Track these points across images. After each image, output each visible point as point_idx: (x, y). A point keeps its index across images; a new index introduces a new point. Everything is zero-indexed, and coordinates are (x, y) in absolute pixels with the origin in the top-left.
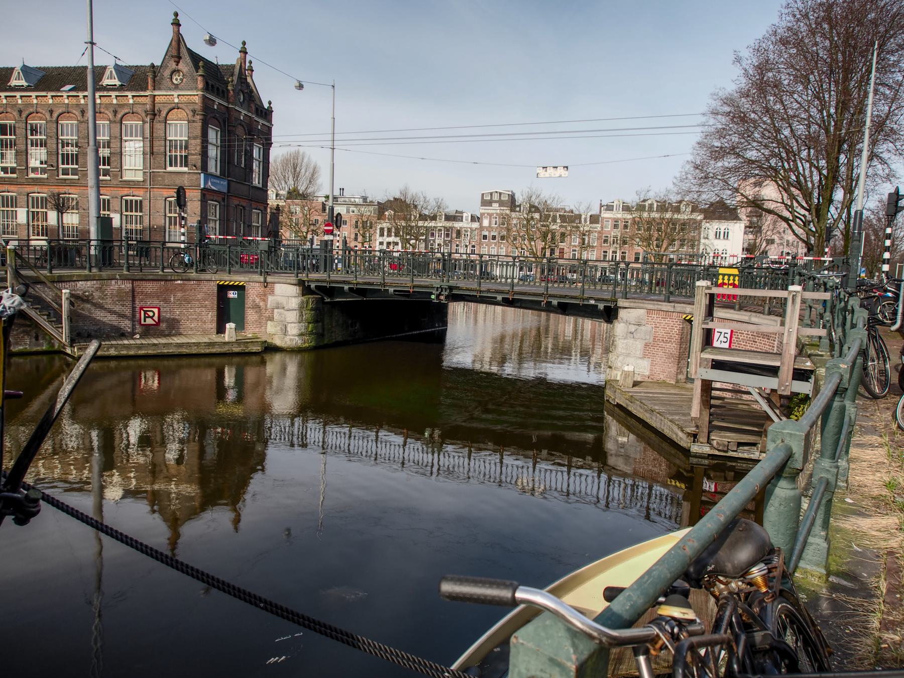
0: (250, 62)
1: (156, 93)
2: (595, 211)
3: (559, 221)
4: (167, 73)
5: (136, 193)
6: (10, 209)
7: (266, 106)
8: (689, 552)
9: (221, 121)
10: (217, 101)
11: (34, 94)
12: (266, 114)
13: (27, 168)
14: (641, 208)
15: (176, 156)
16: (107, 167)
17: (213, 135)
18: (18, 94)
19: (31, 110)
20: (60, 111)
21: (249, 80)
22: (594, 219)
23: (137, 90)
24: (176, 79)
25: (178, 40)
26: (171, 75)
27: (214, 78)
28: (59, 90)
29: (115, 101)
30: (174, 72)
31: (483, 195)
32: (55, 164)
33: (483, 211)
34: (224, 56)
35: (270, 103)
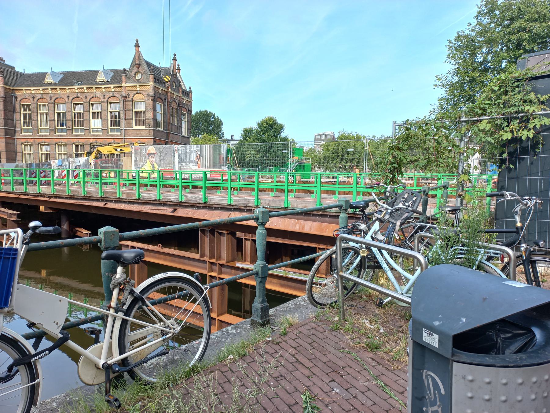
0: (179, 65)
5: (99, 141)
7: (188, 90)
9: (163, 99)
10: (161, 88)
11: (58, 88)
12: (187, 94)
15: (139, 120)
16: (118, 127)
17: (159, 106)
18: (49, 88)
19: (57, 96)
20: (73, 97)
21: (178, 76)
24: (138, 77)
25: (138, 55)
27: (156, 74)
28: (73, 85)
30: (137, 73)
31: (315, 136)
32: (71, 127)
33: (315, 146)
34: (162, 61)
35: (190, 88)
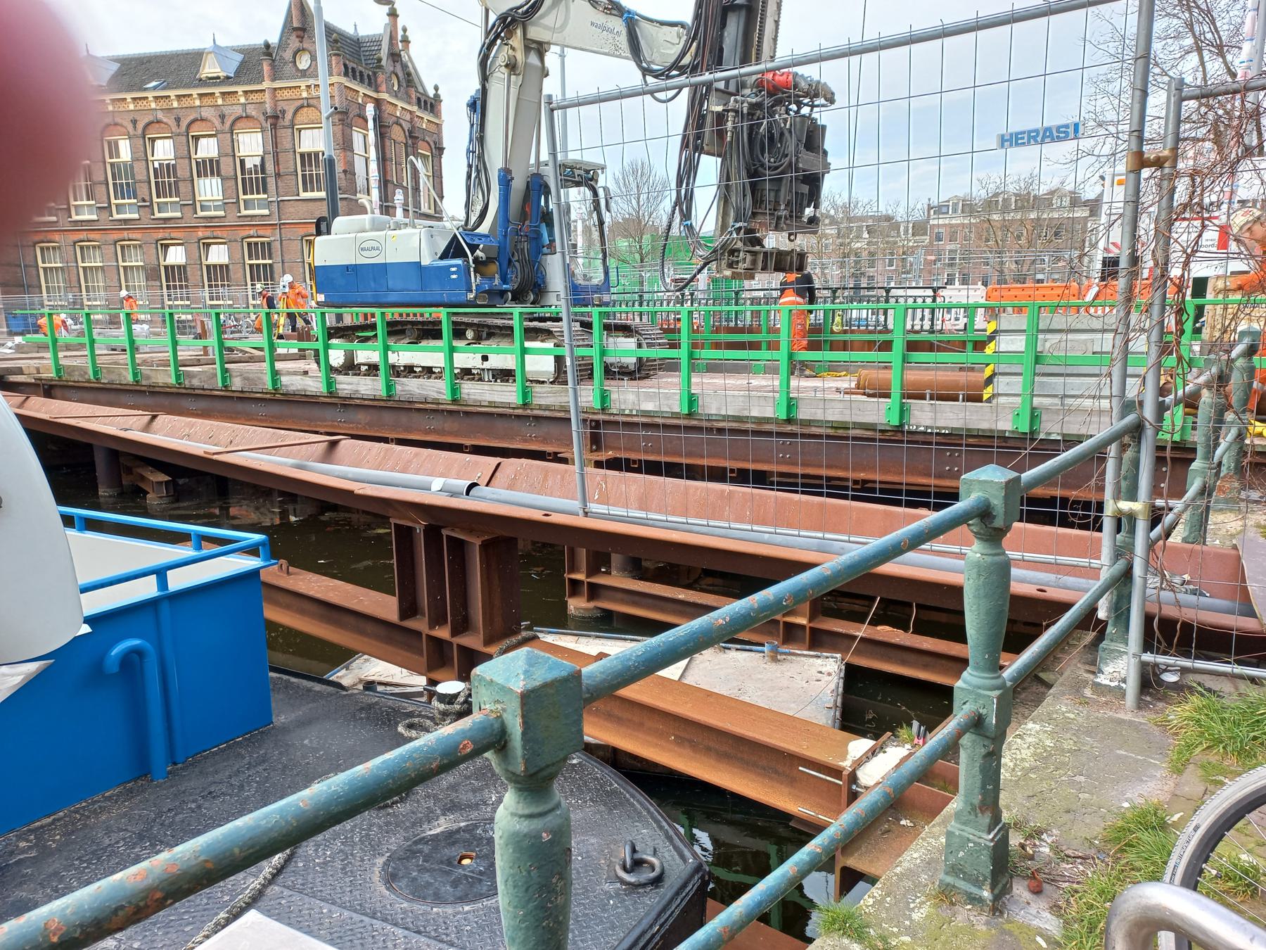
0: (405, 30)
1: (278, 84)
2: (918, 215)
3: (866, 235)
4: (288, 55)
6: (261, 261)
7: (431, 93)
8: (596, 720)
13: (194, 204)
14: (990, 204)
15: (311, 175)
20: (147, 121)
22: (919, 228)
23: (250, 82)
26: (294, 57)
27: (356, 58)
29: (175, 104)
32: (147, 198)
35: (436, 88)
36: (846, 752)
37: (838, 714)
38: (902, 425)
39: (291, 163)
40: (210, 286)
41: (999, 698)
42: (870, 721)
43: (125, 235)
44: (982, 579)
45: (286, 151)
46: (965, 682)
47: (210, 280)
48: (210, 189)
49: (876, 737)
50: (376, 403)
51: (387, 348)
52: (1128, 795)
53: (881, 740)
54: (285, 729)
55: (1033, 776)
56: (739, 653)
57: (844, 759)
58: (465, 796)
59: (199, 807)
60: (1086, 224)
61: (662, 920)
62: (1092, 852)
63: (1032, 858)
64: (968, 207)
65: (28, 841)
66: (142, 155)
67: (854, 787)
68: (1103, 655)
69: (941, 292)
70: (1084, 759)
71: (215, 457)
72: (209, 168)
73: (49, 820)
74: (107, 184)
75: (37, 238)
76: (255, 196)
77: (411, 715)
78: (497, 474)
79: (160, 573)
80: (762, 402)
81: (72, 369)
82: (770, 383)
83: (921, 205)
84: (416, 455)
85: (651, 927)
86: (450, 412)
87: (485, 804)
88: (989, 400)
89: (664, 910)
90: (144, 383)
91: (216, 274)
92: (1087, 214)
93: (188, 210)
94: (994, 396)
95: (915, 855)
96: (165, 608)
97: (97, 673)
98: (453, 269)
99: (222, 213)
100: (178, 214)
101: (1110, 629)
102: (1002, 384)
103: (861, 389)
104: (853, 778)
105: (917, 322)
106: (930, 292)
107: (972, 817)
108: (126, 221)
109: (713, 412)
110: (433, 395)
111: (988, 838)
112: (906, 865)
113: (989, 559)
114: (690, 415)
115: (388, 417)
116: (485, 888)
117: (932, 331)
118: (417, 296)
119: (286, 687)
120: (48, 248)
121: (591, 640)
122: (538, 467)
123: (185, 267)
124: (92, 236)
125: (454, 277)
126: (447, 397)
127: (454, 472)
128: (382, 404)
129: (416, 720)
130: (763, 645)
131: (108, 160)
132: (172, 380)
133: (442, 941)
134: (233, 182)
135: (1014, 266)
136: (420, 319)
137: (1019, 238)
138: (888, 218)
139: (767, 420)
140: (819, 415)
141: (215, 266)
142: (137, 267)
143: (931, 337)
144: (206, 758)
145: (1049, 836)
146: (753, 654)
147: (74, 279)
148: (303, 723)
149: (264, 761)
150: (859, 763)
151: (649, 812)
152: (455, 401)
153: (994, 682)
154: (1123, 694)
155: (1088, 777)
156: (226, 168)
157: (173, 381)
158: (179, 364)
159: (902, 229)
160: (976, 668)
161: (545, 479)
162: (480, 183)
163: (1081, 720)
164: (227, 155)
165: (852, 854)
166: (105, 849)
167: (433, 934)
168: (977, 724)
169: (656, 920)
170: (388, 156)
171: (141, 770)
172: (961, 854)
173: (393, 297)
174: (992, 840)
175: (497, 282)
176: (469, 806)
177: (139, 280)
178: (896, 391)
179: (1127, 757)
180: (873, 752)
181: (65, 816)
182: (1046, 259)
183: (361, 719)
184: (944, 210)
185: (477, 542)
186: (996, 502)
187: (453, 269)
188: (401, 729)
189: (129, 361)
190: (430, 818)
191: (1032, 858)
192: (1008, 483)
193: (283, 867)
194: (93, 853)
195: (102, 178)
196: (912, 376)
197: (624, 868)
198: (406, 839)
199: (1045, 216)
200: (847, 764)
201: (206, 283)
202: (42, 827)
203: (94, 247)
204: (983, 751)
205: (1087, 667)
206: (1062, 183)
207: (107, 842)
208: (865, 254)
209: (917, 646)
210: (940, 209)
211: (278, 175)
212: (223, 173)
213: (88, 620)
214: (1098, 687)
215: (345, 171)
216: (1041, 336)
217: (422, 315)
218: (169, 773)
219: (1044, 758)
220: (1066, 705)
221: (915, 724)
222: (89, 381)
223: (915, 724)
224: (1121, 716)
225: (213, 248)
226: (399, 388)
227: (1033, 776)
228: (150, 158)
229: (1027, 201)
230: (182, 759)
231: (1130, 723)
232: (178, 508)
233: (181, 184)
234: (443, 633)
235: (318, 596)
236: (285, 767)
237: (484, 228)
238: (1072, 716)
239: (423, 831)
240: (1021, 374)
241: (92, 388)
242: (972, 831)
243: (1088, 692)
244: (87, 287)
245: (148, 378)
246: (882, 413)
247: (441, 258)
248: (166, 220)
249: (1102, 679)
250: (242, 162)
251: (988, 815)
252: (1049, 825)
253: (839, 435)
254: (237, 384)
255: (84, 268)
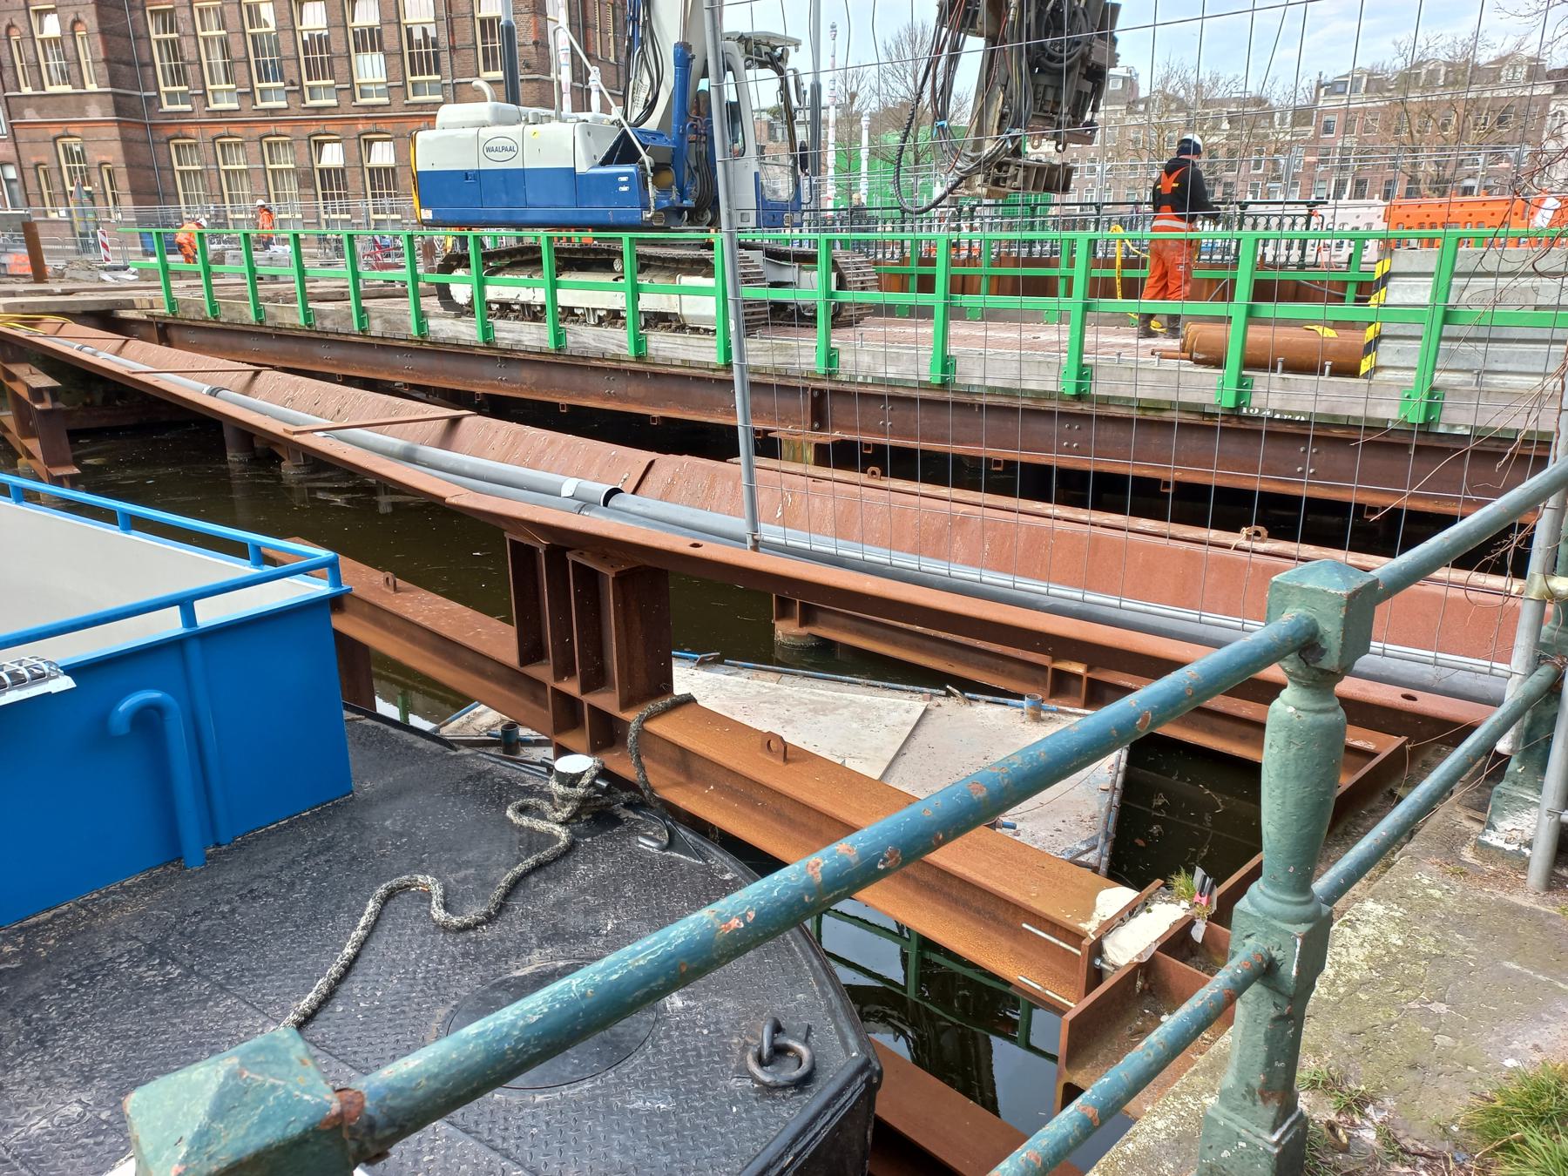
2: (1303, 100)
14: (1407, 79)
22: (1302, 115)
32: (296, 80)
36: (1093, 907)
37: (1115, 798)
38: (1238, 407)
39: (469, 33)
40: (374, 196)
41: (1305, 939)
42: (1158, 809)
43: (272, 128)
44: (1294, 749)
45: (463, 16)
46: (1252, 903)
47: (373, 187)
48: (370, 68)
49: (1139, 885)
50: (543, 358)
51: (555, 286)
52: (1516, 1045)
53: (1147, 891)
54: (368, 803)
55: (1363, 997)
56: (989, 706)
57: (1087, 918)
58: (574, 920)
59: (233, 911)
60: (1547, 105)
61: (799, 1147)
62: (1446, 1147)
63: (1345, 1149)
64: (1376, 83)
65: (15, 944)
66: (289, 23)
67: (1098, 962)
68: (1499, 803)
69: (1320, 210)
70: (1449, 973)
71: (295, 438)
72: (369, 40)
73: (49, 915)
74: (249, 62)
75: (170, 132)
76: (426, 77)
77: (529, 792)
78: (649, 476)
79: (185, 603)
80: (1044, 370)
81: (188, 304)
82: (1055, 338)
83: (1308, 82)
84: (552, 442)
85: (781, 1158)
86: (635, 373)
87: (597, 934)
88: (1365, 376)
89: (803, 1131)
90: (268, 323)
91: (380, 180)
92: (1550, 90)
93: (345, 95)
94: (1376, 369)
95: (1160, 1124)
96: (194, 649)
97: (100, 735)
98: (624, 179)
99: (385, 100)
100: (334, 102)
101: (1513, 766)
102: (1387, 353)
103: (1187, 352)
104: (1097, 949)
105: (1283, 251)
106: (1304, 210)
107: (1248, 1103)
108: (272, 111)
109: (975, 382)
110: (612, 349)
111: (1271, 1140)
112: (1142, 1140)
113: (1308, 718)
114: (944, 385)
115: (558, 376)
116: (569, 1069)
117: (1301, 266)
118: (570, 213)
119: (381, 742)
120: (184, 146)
121: (797, 679)
122: (703, 468)
123: (343, 170)
124: (234, 130)
125: (625, 189)
126: (629, 352)
127: (594, 470)
128: (550, 359)
129: (532, 801)
130: (1021, 697)
131: (249, 31)
132: (300, 321)
133: (494, 1149)
134: (398, 59)
135: (1432, 169)
136: (565, 245)
137: (1444, 127)
138: (1260, 101)
139: (1049, 395)
140: (1125, 391)
141: (379, 170)
142: (288, 170)
143: (1301, 276)
144: (258, 838)
145: (1379, 1109)
146: (1007, 709)
147: (216, 185)
148: (392, 795)
149: (328, 849)
150: (1109, 927)
151: (811, 966)
152: (639, 358)
153: (1300, 910)
154: (1525, 864)
155: (1453, 1005)
156: (390, 41)
157: (301, 321)
158: (307, 297)
159: (1277, 115)
160: (1274, 884)
161: (711, 487)
162: (644, 59)
163: (1451, 902)
164: (390, 22)
165: (1082, 1066)
166: (102, 965)
167: (486, 1136)
168: (1267, 971)
169: (790, 1147)
170: (591, 21)
171: (174, 855)
172: (1225, 1154)
173: (534, 215)
174: (1277, 1144)
175: (674, 196)
176: (575, 936)
177: (291, 187)
178: (1233, 359)
179: (1521, 975)
180: (1132, 911)
181: (70, 911)
182: (1481, 161)
183: (465, 793)
184: (1340, 88)
185: (610, 574)
186: (1328, 627)
187: (624, 179)
188: (510, 813)
189: (250, 294)
190: (520, 952)
191: (1345, 1149)
192: (1352, 597)
193: (315, 1012)
194: (87, 969)
195: (193, 58)
196: (1259, 334)
197: (761, 1062)
198: (484, 981)
199: (1488, 94)
200: (1090, 927)
201: (320, 192)
202: (37, 925)
203: (237, 145)
204: (1273, 1012)
205: (1471, 813)
206: (1519, 45)
207: (109, 954)
208: (1222, 152)
209: (1233, 711)
210: (1333, 88)
211: (453, 49)
212: (386, 46)
213: (70, 670)
214: (1483, 848)
215: (536, 43)
216: (1457, 281)
217: (569, 239)
218: (208, 857)
219: (1384, 963)
220: (1430, 874)
221: (1199, 872)
222: (206, 320)
223: (1199, 872)
224: (1518, 899)
225: (327, 147)
226: (570, 338)
227: (1363, 997)
228: (298, 27)
229: (1464, 72)
230: (225, 844)
231: (1532, 911)
232: (318, 480)
233: (335, 61)
234: (572, 687)
235: (426, 624)
236: (354, 858)
237: (652, 124)
238: (1438, 894)
239: (508, 971)
240: (1420, 338)
241: (211, 329)
242: (1246, 1123)
243: (1467, 854)
244: (231, 196)
245: (273, 317)
246: (1211, 389)
247: (603, 163)
248: (319, 109)
249: (1493, 839)
250: (409, 32)
251: (1275, 1103)
252: (1379, 1088)
253: (1151, 421)
254: (376, 328)
255: (227, 172)
